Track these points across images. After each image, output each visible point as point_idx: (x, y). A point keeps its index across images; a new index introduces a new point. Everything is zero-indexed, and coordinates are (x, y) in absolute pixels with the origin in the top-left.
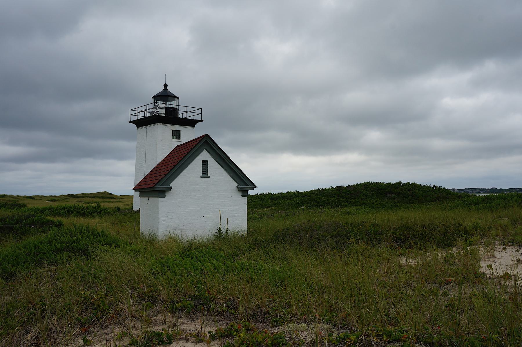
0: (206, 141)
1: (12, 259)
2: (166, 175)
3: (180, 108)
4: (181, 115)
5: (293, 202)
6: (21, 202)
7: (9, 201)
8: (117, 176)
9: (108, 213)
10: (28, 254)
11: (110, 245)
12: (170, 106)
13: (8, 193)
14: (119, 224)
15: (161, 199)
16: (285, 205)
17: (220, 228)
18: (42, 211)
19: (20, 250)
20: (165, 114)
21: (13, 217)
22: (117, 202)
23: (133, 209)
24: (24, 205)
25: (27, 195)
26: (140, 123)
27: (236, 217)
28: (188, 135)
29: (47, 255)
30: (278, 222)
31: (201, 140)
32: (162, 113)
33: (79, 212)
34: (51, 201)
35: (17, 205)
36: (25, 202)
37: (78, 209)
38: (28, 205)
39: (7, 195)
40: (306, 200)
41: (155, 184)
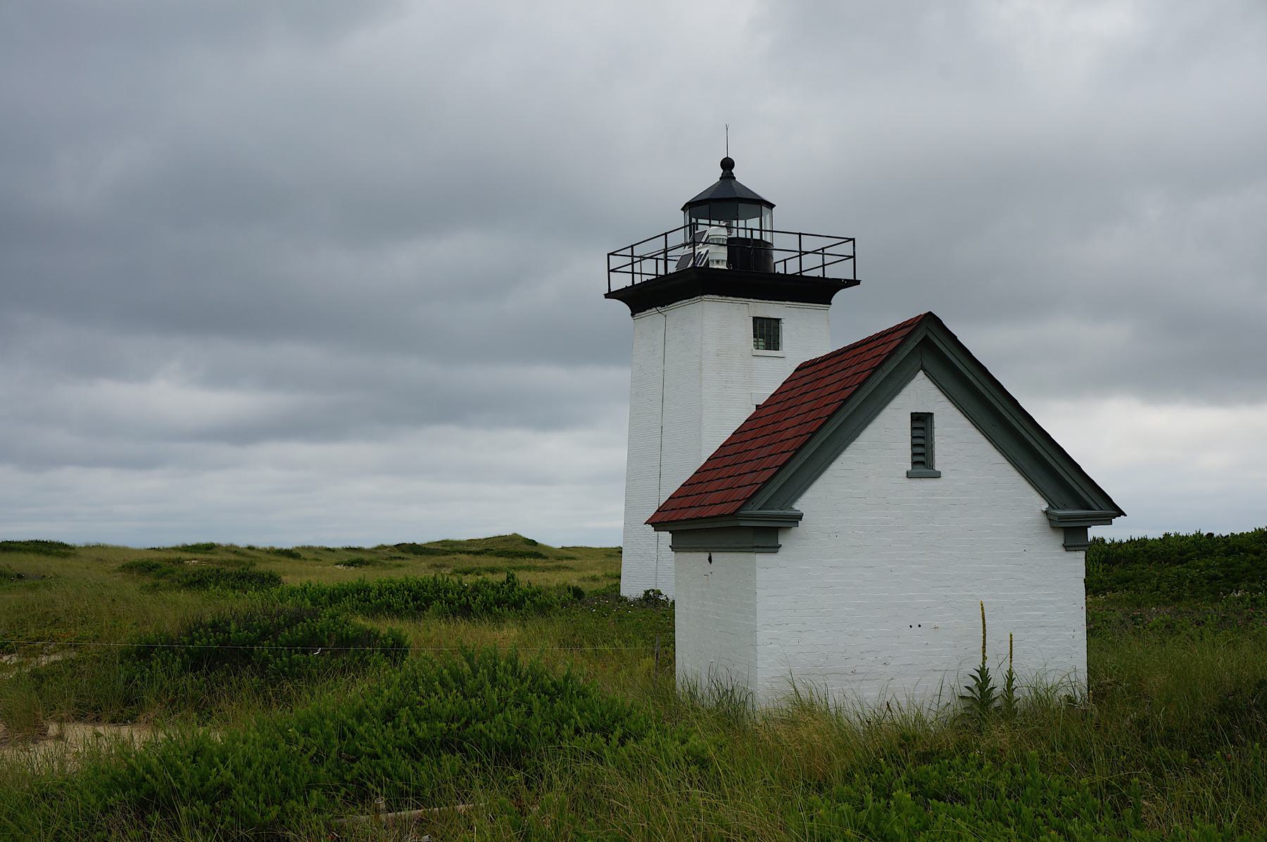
0: (926, 342)
1: (266, 773)
2: (782, 467)
3: (778, 241)
4: (784, 263)
5: (1195, 572)
6: (261, 568)
7: (228, 563)
8: (571, 473)
9: (544, 609)
10: (318, 760)
11: (606, 732)
12: (742, 234)
13: (222, 540)
14: (589, 649)
15: (761, 559)
16: (1164, 585)
17: (983, 672)
18: (335, 597)
19: (289, 741)
20: (729, 262)
21: (251, 618)
22: (559, 568)
23: (624, 592)
24: (273, 579)
25: (278, 546)
26: (642, 298)
27: (1045, 632)
28: (811, 334)
29: (387, 763)
30: (1217, 655)
31: (906, 338)
32: (718, 257)
33: (450, 602)
34: (351, 564)
35: (251, 577)
36: (277, 566)
37: (446, 591)
38: (284, 578)
39: (219, 546)
40: (1245, 565)
41: (738, 500)
